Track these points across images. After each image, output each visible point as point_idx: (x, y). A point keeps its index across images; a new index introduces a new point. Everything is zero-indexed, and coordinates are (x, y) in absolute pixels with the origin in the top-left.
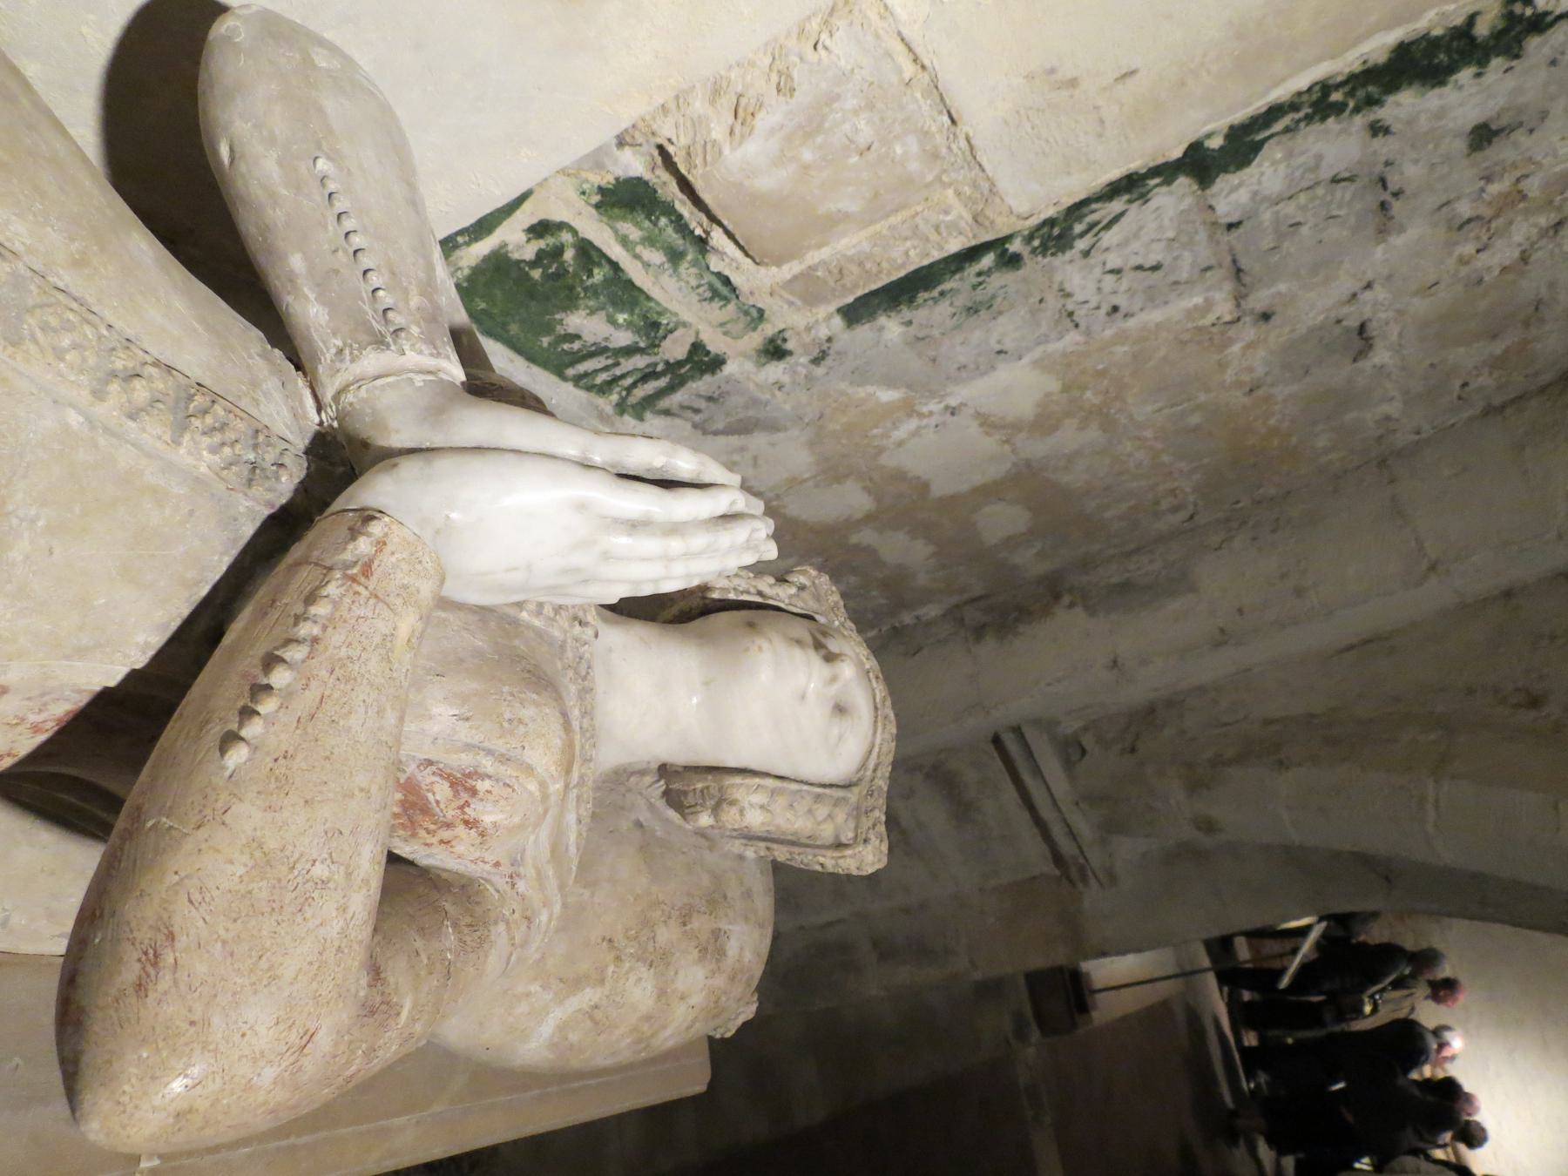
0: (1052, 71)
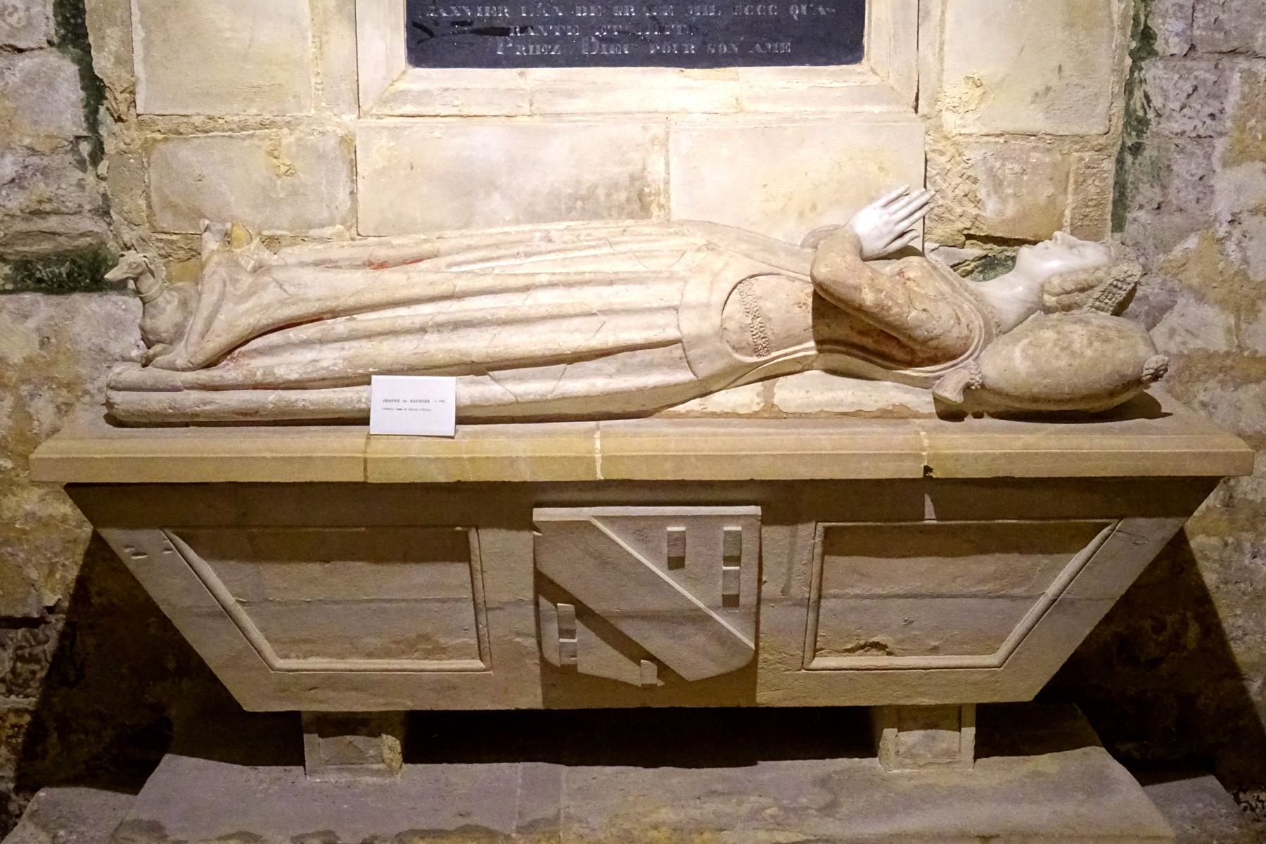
0: (1037, 94)
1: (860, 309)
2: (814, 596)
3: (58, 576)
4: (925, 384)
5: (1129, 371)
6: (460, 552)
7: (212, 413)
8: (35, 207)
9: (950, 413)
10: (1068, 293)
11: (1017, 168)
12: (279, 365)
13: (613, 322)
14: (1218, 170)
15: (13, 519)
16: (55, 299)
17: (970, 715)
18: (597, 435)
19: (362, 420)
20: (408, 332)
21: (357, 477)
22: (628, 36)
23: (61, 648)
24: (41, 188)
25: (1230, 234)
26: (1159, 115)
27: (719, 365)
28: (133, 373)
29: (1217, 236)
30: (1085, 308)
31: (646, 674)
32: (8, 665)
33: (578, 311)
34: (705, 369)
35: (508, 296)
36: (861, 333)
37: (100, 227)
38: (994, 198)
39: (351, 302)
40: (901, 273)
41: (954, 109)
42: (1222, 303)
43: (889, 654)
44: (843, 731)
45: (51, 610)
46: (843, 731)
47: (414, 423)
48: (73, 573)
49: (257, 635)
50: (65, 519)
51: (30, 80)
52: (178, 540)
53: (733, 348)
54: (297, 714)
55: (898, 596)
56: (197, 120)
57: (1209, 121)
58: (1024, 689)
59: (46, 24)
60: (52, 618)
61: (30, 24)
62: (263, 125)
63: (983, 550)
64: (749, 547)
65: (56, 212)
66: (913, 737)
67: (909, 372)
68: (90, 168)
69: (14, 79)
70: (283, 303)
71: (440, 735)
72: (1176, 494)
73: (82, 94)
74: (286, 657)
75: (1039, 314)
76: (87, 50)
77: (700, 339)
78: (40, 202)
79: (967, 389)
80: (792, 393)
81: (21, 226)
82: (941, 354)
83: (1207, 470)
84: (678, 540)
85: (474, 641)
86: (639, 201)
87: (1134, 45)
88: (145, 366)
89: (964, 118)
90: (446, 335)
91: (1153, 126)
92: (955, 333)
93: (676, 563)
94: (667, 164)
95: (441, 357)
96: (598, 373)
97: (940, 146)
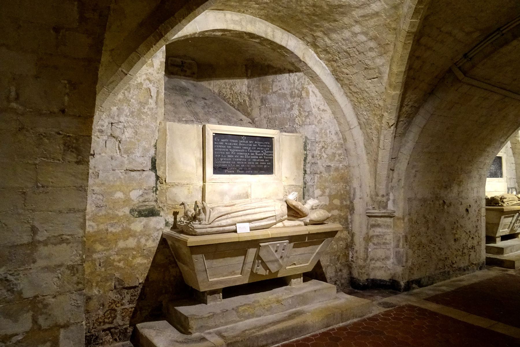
9: (306, 224)
15: (135, 265)
16: (146, 218)
17: (302, 275)
19: (235, 231)
21: (238, 240)
22: (243, 170)
23: (141, 292)
24: (146, 197)
29: (190, 214)
32: (129, 298)
37: (154, 203)
44: (282, 282)
45: (140, 284)
47: (244, 230)
48: (146, 275)
50: (145, 263)
51: (146, 176)
58: (310, 269)
59: (150, 166)
61: (147, 166)
63: (310, 245)
66: (295, 280)
69: (143, 176)
71: (230, 292)
76: (156, 171)
81: (141, 204)
83: (337, 230)
84: (278, 247)
86: (247, 196)
95: (246, 220)
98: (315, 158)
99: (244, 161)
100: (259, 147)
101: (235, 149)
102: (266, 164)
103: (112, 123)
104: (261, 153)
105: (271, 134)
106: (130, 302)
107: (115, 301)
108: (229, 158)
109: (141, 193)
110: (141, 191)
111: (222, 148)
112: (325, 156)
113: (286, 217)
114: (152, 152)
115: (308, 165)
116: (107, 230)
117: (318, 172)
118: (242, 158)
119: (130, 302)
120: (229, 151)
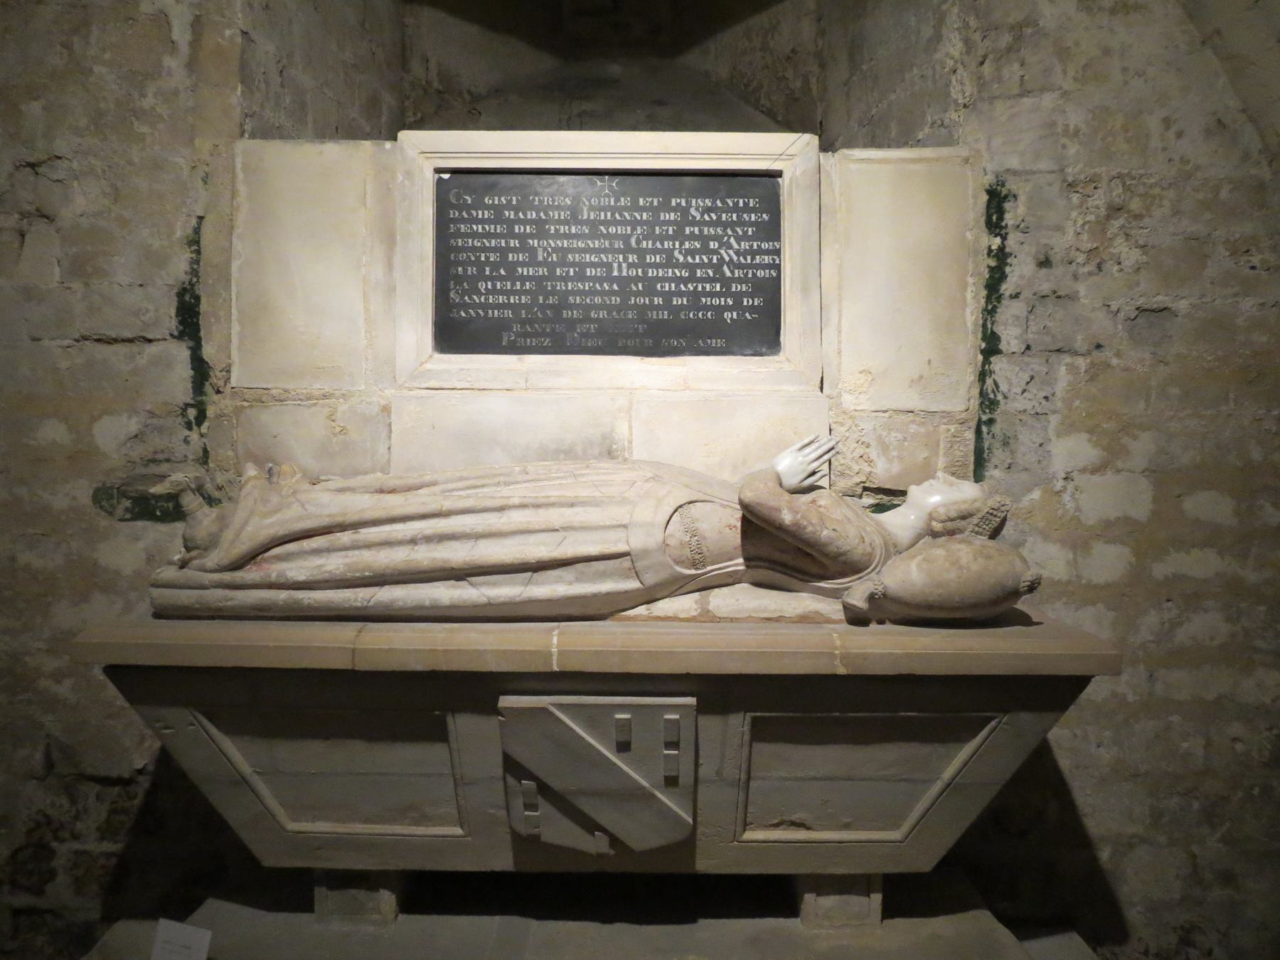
1: (781, 528)
2: (743, 776)
3: (146, 745)
4: (834, 594)
5: (1010, 583)
6: (439, 734)
7: (233, 608)
8: (150, 457)
9: (857, 619)
10: (952, 520)
11: (900, 436)
12: (291, 569)
13: (572, 537)
14: (1053, 438)
18: (556, 632)
20: (400, 543)
24: (157, 442)
25: (1065, 488)
26: (1005, 397)
27: (662, 575)
28: (170, 573)
30: (967, 533)
31: (596, 845)
32: (104, 815)
33: (543, 527)
34: (650, 579)
35: (486, 515)
36: (782, 551)
38: (883, 459)
39: (353, 517)
40: (814, 502)
41: (850, 392)
42: (1063, 542)
43: (808, 829)
44: (772, 894)
46: (772, 894)
49: (272, 803)
52: (201, 718)
53: (674, 561)
54: (309, 871)
55: (814, 778)
56: (274, 392)
57: (1044, 402)
58: (924, 862)
59: (170, 322)
60: (141, 779)
62: (325, 396)
64: (687, 736)
65: (168, 460)
66: (829, 901)
67: (822, 584)
68: (195, 427)
69: (142, 361)
70: (301, 518)
72: (1054, 691)
73: (192, 373)
74: (295, 820)
75: (928, 539)
77: (645, 552)
78: (156, 453)
79: (872, 598)
80: (723, 601)
81: (141, 470)
82: (848, 567)
85: (455, 811)
87: (983, 345)
88: (182, 567)
89: (858, 398)
90: (432, 546)
91: (1002, 406)
92: (860, 550)
93: (623, 747)
94: (630, 427)
96: (559, 580)
97: (840, 419)
98: (1058, 271)
99: (602, 293)
100: (694, 223)
101: (558, 236)
102: (738, 306)
103: (32, 166)
104: (706, 250)
105: (763, 156)
106: (106, 832)
107: (49, 821)
108: (523, 279)
109: (133, 426)
110: (135, 419)
111: (488, 235)
112: (1131, 256)
113: (738, 564)
114: (179, 266)
115: (1010, 311)
116: (13, 559)
117: (1080, 343)
118: (594, 279)
119: (106, 832)
120: (524, 248)
